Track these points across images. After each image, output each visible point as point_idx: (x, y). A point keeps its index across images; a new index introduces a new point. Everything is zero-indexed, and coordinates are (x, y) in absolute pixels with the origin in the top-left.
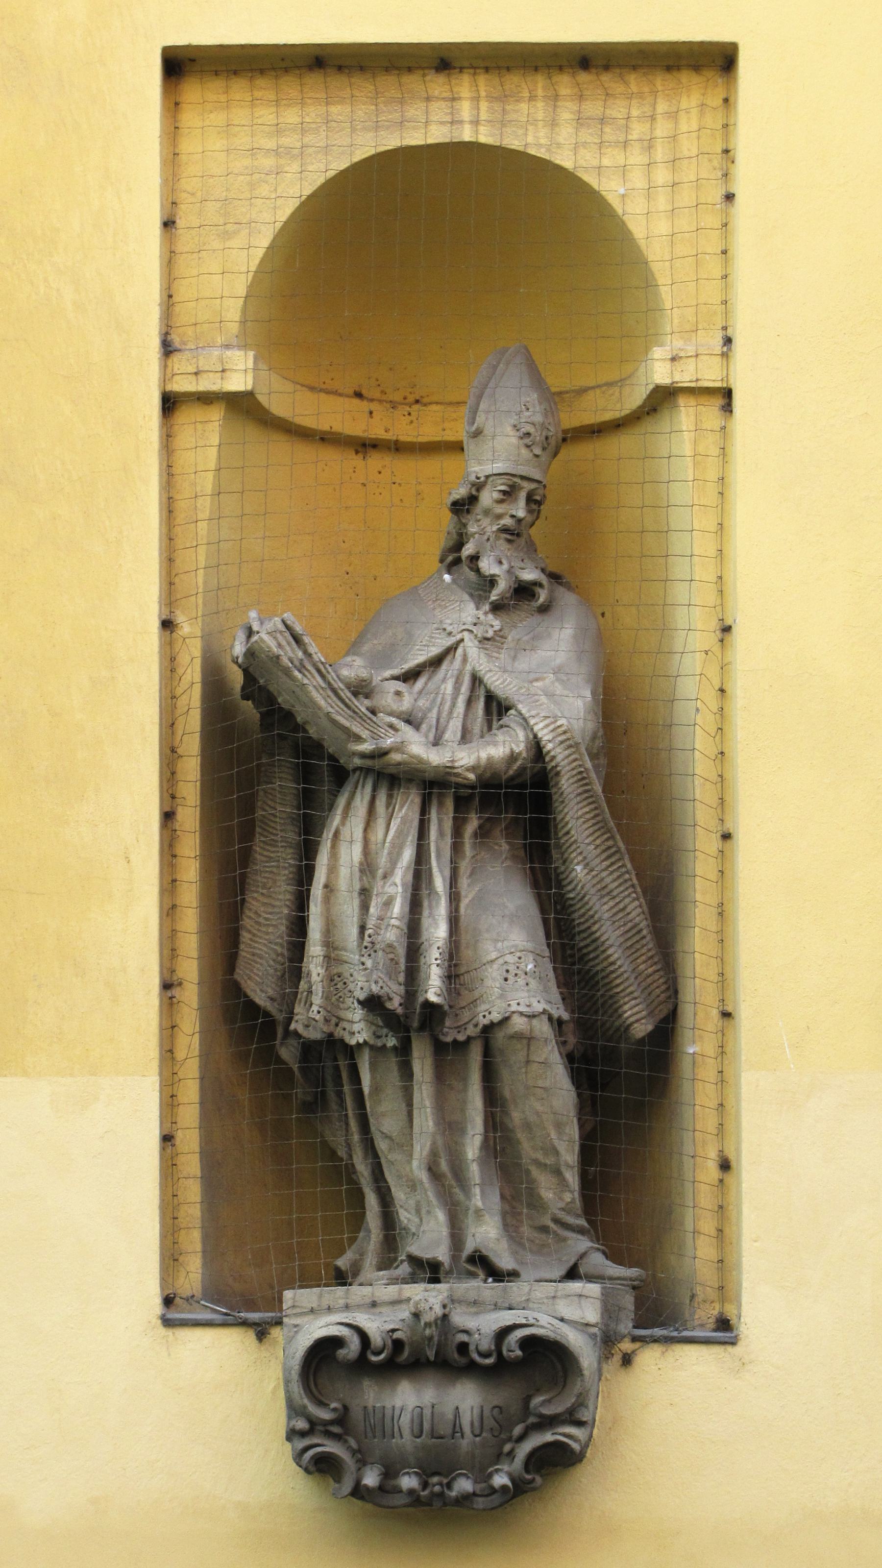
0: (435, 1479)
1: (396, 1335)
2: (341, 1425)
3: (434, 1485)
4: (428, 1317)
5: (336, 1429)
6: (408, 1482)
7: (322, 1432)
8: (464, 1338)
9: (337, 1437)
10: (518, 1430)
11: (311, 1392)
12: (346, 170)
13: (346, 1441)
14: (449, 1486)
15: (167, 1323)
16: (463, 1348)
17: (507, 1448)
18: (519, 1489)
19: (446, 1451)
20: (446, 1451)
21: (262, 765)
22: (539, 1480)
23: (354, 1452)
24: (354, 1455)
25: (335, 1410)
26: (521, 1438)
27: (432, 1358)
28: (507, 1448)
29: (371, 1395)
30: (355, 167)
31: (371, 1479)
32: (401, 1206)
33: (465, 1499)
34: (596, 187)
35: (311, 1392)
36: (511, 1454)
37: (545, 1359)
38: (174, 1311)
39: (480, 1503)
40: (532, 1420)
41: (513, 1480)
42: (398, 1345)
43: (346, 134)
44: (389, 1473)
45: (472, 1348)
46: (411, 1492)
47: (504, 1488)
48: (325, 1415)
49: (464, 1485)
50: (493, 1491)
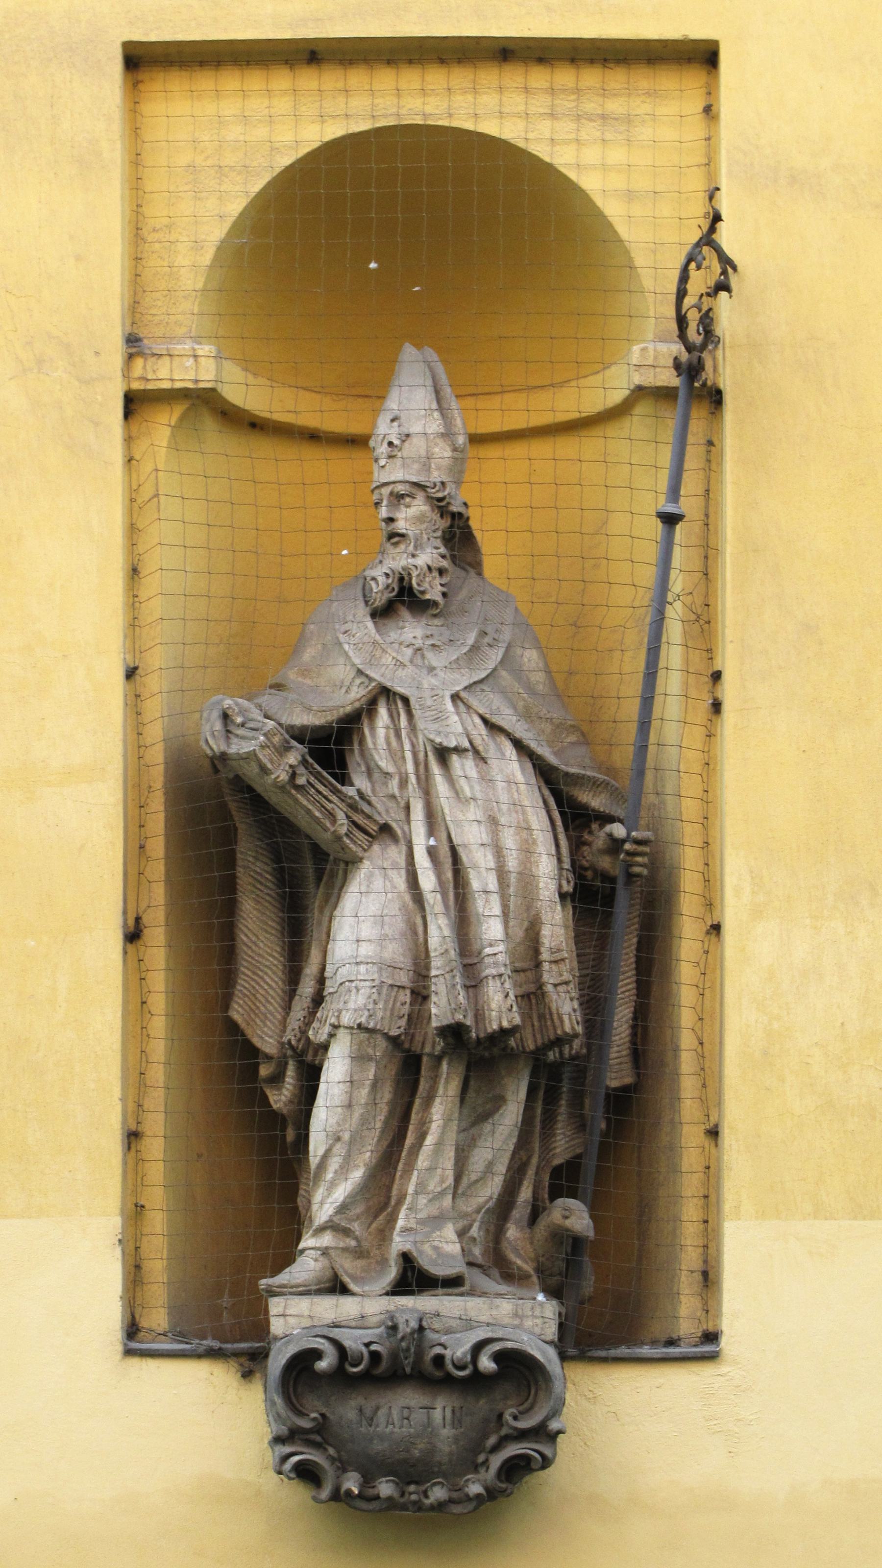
0: (412, 1488)
1: (373, 1347)
2: (320, 1434)
3: (410, 1494)
4: (403, 1329)
5: (318, 1439)
6: (385, 1488)
7: (302, 1440)
8: (438, 1350)
9: (317, 1446)
10: (492, 1440)
11: (291, 1403)
12: (292, 166)
13: (326, 1450)
14: (426, 1494)
15: (129, 1352)
16: (439, 1360)
17: (481, 1458)
18: (491, 1494)
19: (418, 1450)
20: (418, 1450)
21: (241, 843)
22: (510, 1486)
23: (332, 1460)
24: (333, 1464)
25: (314, 1419)
26: (495, 1449)
27: (408, 1370)
28: (481, 1458)
29: (347, 1410)
30: (299, 161)
31: (352, 1483)
32: (435, 1003)
33: (440, 1506)
34: (547, 159)
35: (291, 1403)
36: (486, 1462)
37: (518, 1371)
38: (135, 1339)
39: (456, 1509)
40: (504, 1431)
41: (487, 1489)
42: (375, 1357)
43: (288, 125)
44: (367, 1480)
45: (448, 1361)
46: (390, 1499)
47: (478, 1496)
48: (305, 1424)
49: (438, 1493)
50: (468, 1498)
